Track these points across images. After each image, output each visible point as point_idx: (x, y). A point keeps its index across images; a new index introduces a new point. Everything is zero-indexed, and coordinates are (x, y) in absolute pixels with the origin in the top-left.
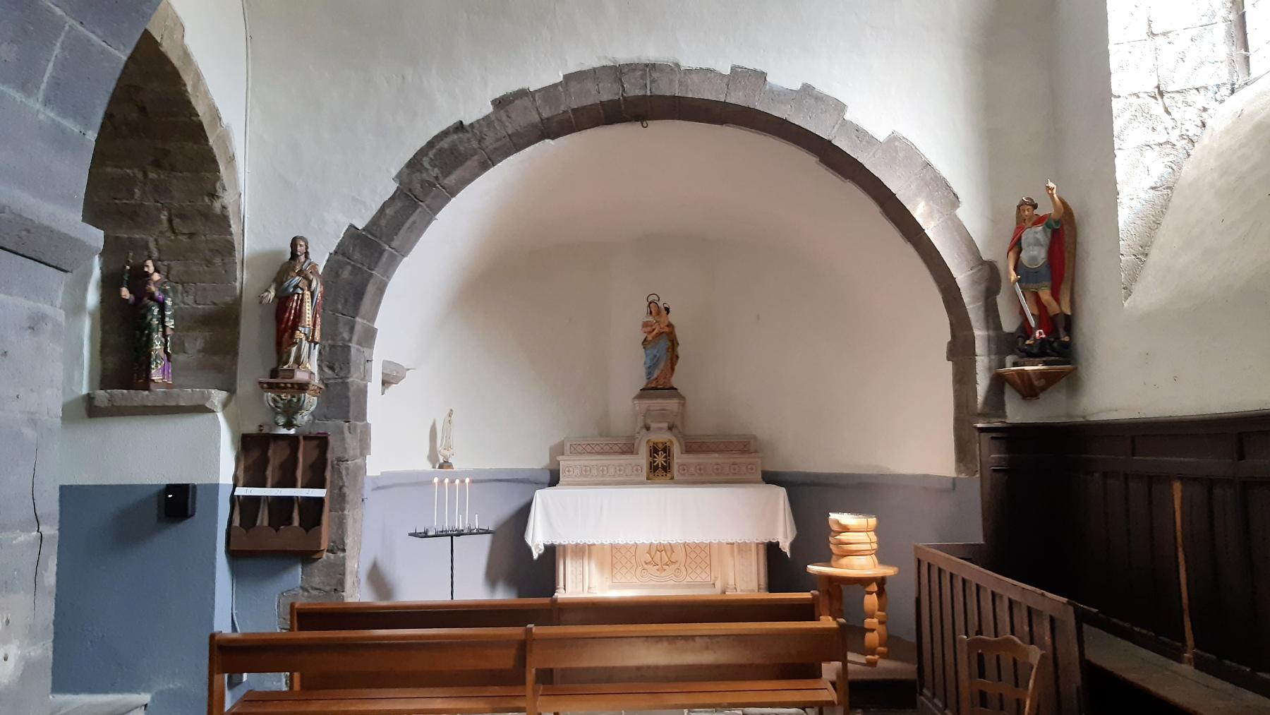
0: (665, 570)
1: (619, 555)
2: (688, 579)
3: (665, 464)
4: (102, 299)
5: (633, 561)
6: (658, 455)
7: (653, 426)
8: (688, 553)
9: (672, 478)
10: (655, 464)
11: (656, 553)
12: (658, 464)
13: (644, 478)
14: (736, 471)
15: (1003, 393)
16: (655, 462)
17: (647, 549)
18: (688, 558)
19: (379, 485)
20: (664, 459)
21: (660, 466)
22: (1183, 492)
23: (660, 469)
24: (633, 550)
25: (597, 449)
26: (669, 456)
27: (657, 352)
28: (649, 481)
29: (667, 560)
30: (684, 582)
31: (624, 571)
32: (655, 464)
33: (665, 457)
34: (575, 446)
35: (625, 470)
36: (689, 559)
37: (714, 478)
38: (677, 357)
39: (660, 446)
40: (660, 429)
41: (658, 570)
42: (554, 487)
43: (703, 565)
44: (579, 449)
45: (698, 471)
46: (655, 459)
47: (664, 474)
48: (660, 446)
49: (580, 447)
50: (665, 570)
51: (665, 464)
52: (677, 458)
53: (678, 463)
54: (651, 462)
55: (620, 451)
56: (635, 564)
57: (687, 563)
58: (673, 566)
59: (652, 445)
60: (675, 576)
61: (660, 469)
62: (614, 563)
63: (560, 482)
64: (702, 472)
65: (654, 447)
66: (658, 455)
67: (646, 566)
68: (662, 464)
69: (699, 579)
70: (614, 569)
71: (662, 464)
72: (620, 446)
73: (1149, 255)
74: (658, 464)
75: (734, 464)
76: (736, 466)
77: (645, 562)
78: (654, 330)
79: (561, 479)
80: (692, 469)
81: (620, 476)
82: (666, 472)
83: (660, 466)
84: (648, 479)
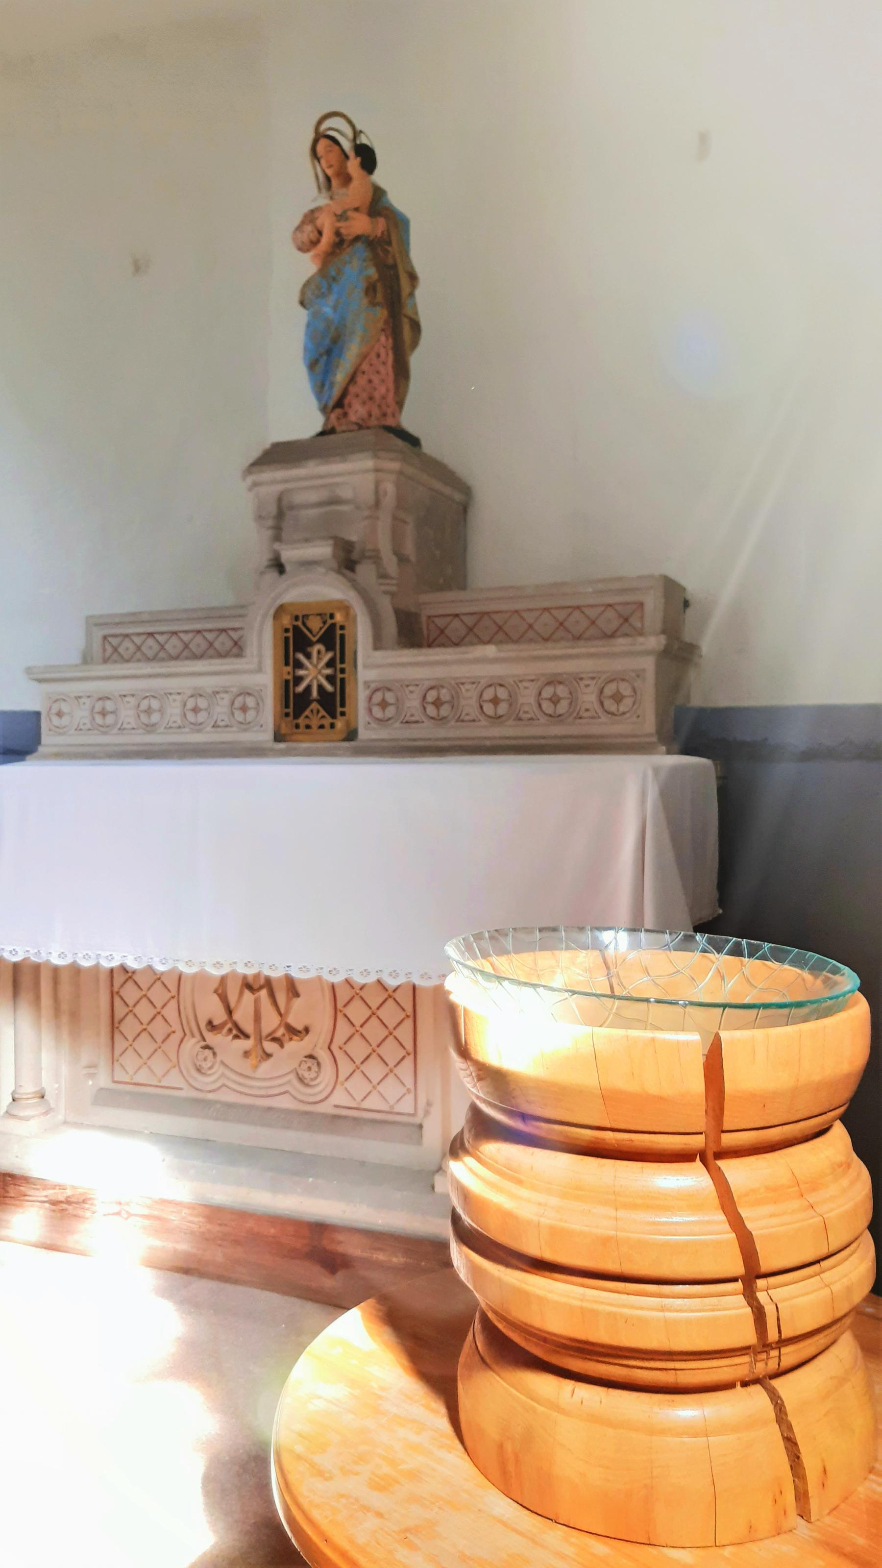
0: (269, 1056)
1: (130, 993)
2: (340, 1098)
3: (329, 688)
5: (170, 1012)
6: (308, 656)
7: (289, 554)
8: (340, 1005)
9: (351, 735)
10: (301, 688)
11: (241, 993)
12: (308, 688)
13: (266, 736)
14: (562, 707)
15: (40, 1049)
16: (298, 680)
17: (215, 985)
18: (341, 1021)
20: (329, 671)
21: (315, 693)
23: (315, 706)
24: (173, 986)
26: (342, 661)
28: (282, 746)
30: (326, 1108)
31: (145, 1045)
33: (330, 664)
35: (161, 711)
37: (426, 732)
38: (416, 327)
39: (315, 624)
40: (308, 564)
41: (246, 1054)
42: (23, 763)
43: (391, 1051)
45: (431, 710)
46: (301, 672)
47: (327, 721)
48: (315, 624)
50: (269, 1056)
51: (329, 688)
53: (367, 684)
54: (287, 682)
56: (176, 1026)
57: (339, 1040)
58: (293, 1046)
59: (287, 621)
60: (301, 1080)
61: (315, 706)
62: (118, 1016)
63: (41, 749)
64: (445, 711)
65: (296, 628)
66: (308, 656)
68: (320, 687)
69: (373, 1102)
70: (117, 1036)
71: (320, 687)
73: (339, 1050)
74: (308, 688)
75: (554, 681)
76: (561, 691)
77: (210, 1023)
79: (45, 739)
80: (413, 703)
81: (197, 727)
82: (334, 716)
83: (315, 693)
84: (279, 737)
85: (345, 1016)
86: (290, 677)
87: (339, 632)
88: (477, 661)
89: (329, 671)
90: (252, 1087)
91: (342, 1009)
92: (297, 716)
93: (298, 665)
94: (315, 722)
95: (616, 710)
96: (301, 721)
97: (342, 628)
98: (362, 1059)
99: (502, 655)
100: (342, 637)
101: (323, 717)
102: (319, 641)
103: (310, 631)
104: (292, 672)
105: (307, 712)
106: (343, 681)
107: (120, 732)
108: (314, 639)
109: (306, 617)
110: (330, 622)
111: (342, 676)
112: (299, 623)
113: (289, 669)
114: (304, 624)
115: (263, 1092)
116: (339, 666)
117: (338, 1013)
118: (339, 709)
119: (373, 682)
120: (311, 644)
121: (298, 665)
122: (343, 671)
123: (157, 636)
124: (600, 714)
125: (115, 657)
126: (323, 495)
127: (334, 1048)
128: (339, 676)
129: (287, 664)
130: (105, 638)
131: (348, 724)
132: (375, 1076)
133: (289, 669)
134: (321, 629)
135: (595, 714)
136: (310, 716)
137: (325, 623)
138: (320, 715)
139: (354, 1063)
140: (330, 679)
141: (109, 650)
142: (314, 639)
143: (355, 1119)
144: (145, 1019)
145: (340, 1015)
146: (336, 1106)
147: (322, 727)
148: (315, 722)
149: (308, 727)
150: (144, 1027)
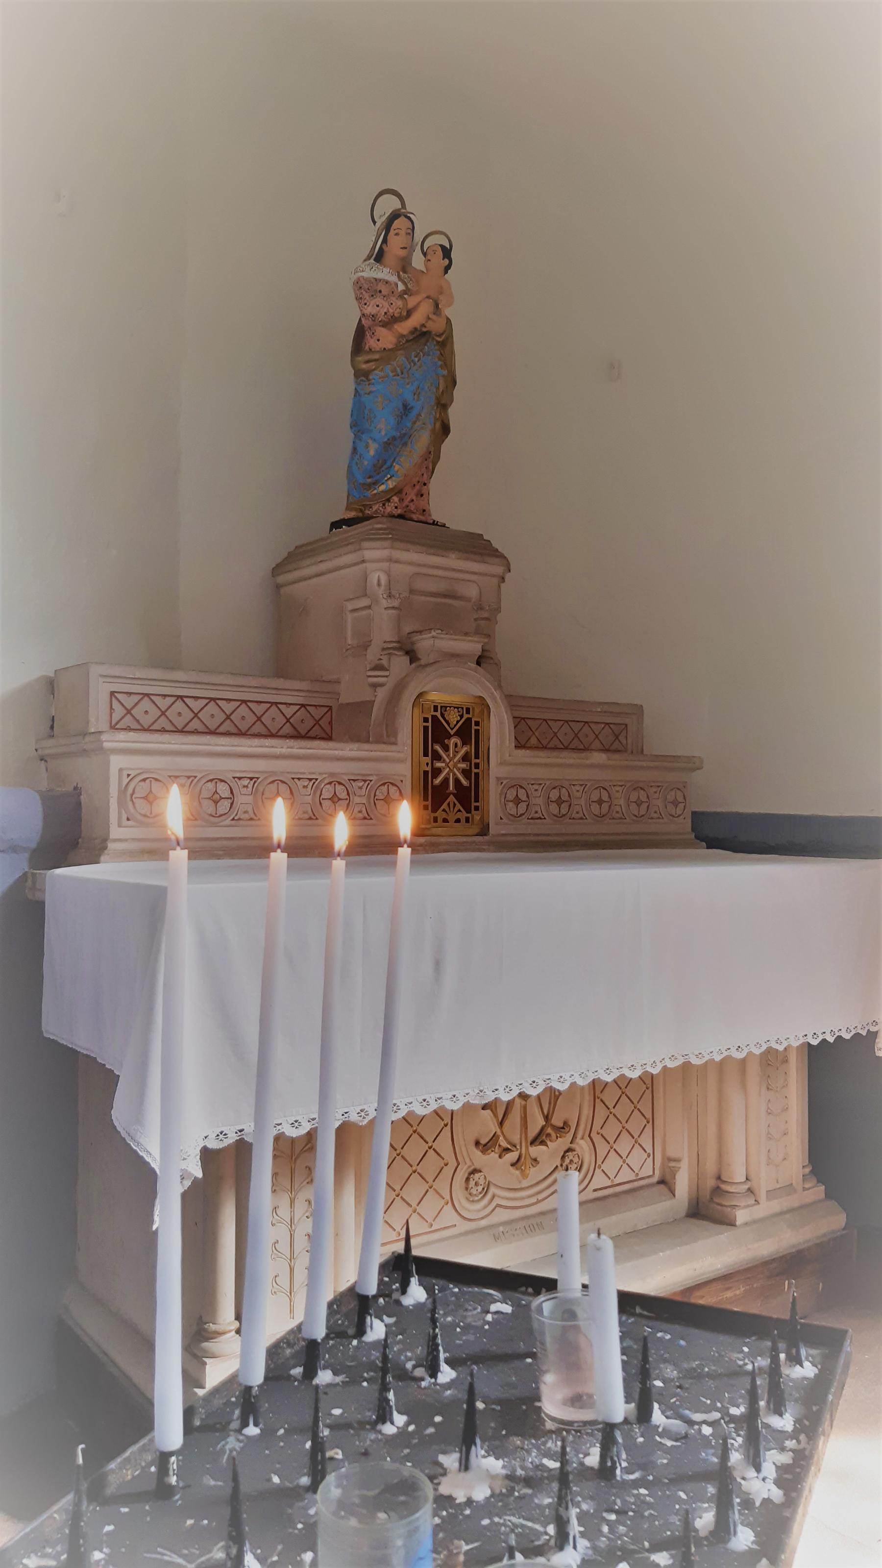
3: (465, 782)
4: (250, 1436)
6: (446, 748)
7: (425, 643)
9: (484, 831)
10: (437, 781)
12: (446, 780)
16: (437, 772)
19: (311, 1423)
20: (463, 766)
22: (269, 825)
24: (649, 1082)
25: (211, 715)
26: (477, 757)
27: (417, 394)
29: (542, 1122)
32: (437, 781)
33: (466, 758)
34: (129, 702)
36: (601, 1113)
39: (453, 717)
44: (146, 711)
47: (463, 815)
48: (453, 717)
49: (146, 704)
52: (503, 763)
55: (287, 729)
61: (452, 798)
66: (446, 748)
67: (479, 1158)
68: (457, 781)
69: (626, 1175)
71: (457, 781)
72: (289, 711)
78: (409, 313)
80: (539, 801)
82: (469, 812)
85: (602, 1101)
86: (429, 769)
87: (474, 727)
88: (592, 766)
89: (463, 766)
90: (523, 1198)
91: (599, 1095)
92: (434, 810)
93: (436, 757)
94: (452, 818)
95: (215, 812)
96: (440, 814)
97: (477, 724)
98: (638, 1134)
99: (611, 762)
100: (477, 731)
101: (459, 811)
102: (454, 735)
103: (448, 724)
104: (430, 765)
105: (445, 806)
106: (477, 775)
107: (233, 822)
108: (452, 732)
109: (444, 708)
110: (466, 716)
111: (476, 771)
112: (438, 714)
113: (428, 759)
114: (442, 715)
115: (534, 1200)
116: (474, 761)
117: (597, 1100)
118: (474, 804)
119: (505, 778)
120: (449, 736)
121: (436, 757)
122: (477, 766)
123: (592, 725)
124: (587, 817)
125: (128, 720)
126: (442, 586)
127: (593, 1135)
128: (474, 770)
129: (426, 754)
130: (112, 693)
131: (482, 818)
132: (624, 1151)
133: (428, 759)
134: (458, 722)
135: (367, 815)
136: (447, 810)
137: (461, 716)
138: (456, 810)
139: (609, 1143)
140: (466, 773)
141: (119, 711)
142: (452, 732)
143: (616, 1195)
144: (414, 1158)
145: (597, 1101)
146: (595, 1190)
147: (458, 821)
148: (452, 818)
149: (445, 821)
150: (414, 1168)
